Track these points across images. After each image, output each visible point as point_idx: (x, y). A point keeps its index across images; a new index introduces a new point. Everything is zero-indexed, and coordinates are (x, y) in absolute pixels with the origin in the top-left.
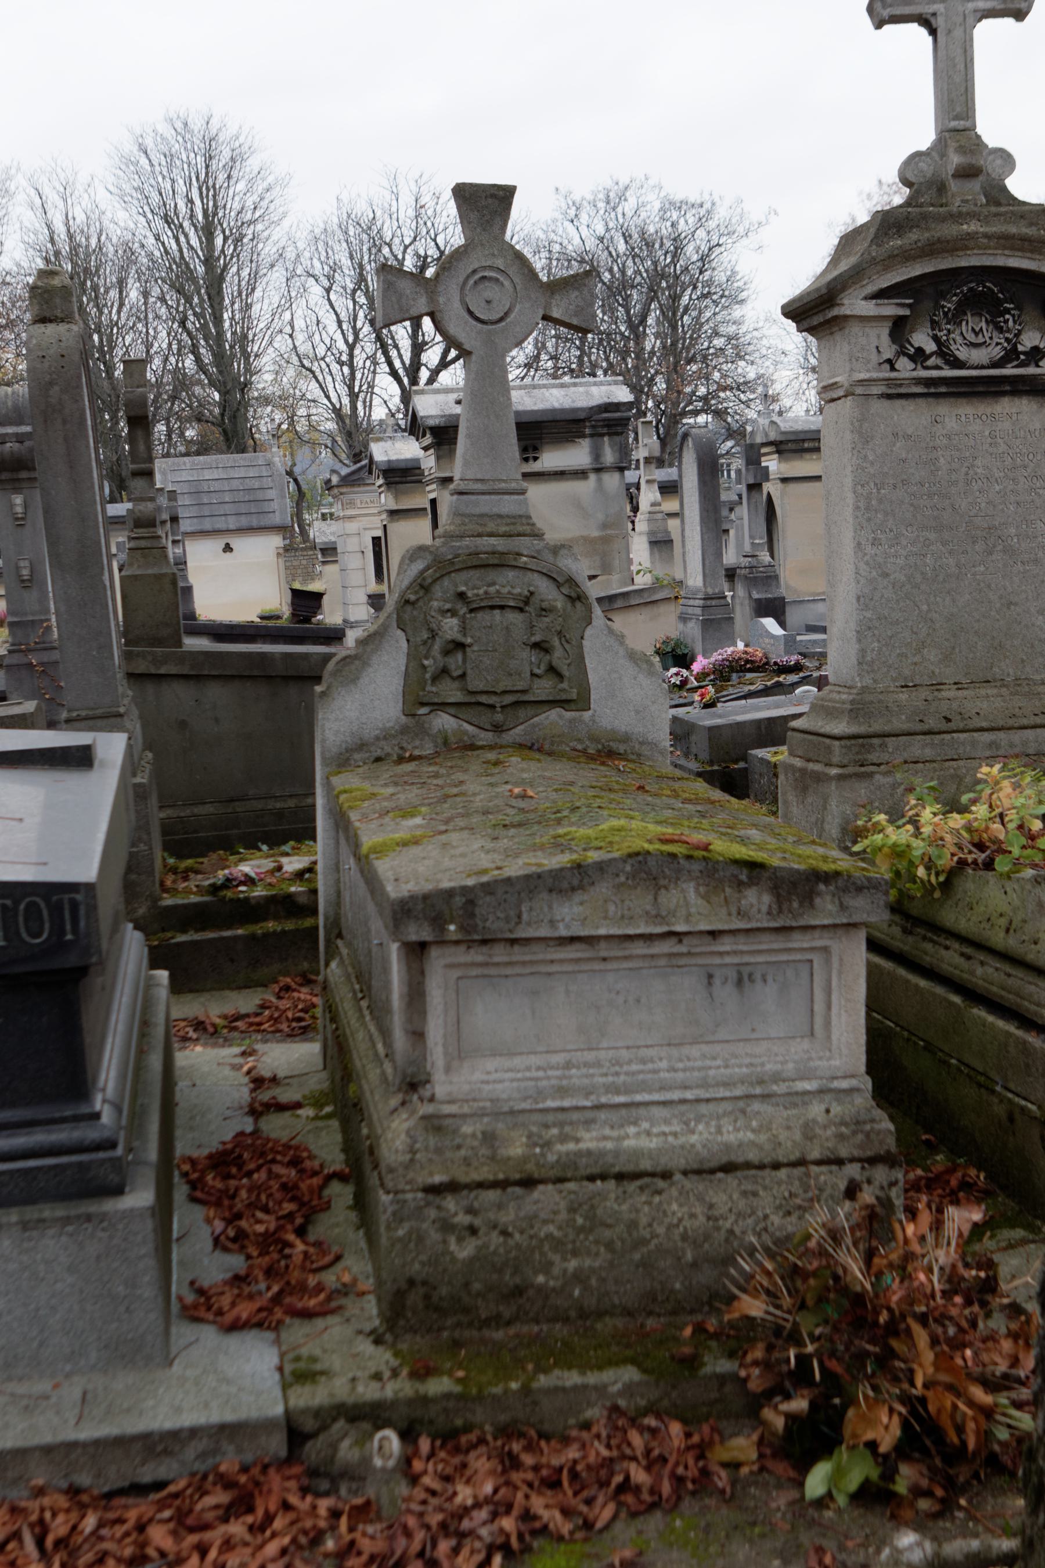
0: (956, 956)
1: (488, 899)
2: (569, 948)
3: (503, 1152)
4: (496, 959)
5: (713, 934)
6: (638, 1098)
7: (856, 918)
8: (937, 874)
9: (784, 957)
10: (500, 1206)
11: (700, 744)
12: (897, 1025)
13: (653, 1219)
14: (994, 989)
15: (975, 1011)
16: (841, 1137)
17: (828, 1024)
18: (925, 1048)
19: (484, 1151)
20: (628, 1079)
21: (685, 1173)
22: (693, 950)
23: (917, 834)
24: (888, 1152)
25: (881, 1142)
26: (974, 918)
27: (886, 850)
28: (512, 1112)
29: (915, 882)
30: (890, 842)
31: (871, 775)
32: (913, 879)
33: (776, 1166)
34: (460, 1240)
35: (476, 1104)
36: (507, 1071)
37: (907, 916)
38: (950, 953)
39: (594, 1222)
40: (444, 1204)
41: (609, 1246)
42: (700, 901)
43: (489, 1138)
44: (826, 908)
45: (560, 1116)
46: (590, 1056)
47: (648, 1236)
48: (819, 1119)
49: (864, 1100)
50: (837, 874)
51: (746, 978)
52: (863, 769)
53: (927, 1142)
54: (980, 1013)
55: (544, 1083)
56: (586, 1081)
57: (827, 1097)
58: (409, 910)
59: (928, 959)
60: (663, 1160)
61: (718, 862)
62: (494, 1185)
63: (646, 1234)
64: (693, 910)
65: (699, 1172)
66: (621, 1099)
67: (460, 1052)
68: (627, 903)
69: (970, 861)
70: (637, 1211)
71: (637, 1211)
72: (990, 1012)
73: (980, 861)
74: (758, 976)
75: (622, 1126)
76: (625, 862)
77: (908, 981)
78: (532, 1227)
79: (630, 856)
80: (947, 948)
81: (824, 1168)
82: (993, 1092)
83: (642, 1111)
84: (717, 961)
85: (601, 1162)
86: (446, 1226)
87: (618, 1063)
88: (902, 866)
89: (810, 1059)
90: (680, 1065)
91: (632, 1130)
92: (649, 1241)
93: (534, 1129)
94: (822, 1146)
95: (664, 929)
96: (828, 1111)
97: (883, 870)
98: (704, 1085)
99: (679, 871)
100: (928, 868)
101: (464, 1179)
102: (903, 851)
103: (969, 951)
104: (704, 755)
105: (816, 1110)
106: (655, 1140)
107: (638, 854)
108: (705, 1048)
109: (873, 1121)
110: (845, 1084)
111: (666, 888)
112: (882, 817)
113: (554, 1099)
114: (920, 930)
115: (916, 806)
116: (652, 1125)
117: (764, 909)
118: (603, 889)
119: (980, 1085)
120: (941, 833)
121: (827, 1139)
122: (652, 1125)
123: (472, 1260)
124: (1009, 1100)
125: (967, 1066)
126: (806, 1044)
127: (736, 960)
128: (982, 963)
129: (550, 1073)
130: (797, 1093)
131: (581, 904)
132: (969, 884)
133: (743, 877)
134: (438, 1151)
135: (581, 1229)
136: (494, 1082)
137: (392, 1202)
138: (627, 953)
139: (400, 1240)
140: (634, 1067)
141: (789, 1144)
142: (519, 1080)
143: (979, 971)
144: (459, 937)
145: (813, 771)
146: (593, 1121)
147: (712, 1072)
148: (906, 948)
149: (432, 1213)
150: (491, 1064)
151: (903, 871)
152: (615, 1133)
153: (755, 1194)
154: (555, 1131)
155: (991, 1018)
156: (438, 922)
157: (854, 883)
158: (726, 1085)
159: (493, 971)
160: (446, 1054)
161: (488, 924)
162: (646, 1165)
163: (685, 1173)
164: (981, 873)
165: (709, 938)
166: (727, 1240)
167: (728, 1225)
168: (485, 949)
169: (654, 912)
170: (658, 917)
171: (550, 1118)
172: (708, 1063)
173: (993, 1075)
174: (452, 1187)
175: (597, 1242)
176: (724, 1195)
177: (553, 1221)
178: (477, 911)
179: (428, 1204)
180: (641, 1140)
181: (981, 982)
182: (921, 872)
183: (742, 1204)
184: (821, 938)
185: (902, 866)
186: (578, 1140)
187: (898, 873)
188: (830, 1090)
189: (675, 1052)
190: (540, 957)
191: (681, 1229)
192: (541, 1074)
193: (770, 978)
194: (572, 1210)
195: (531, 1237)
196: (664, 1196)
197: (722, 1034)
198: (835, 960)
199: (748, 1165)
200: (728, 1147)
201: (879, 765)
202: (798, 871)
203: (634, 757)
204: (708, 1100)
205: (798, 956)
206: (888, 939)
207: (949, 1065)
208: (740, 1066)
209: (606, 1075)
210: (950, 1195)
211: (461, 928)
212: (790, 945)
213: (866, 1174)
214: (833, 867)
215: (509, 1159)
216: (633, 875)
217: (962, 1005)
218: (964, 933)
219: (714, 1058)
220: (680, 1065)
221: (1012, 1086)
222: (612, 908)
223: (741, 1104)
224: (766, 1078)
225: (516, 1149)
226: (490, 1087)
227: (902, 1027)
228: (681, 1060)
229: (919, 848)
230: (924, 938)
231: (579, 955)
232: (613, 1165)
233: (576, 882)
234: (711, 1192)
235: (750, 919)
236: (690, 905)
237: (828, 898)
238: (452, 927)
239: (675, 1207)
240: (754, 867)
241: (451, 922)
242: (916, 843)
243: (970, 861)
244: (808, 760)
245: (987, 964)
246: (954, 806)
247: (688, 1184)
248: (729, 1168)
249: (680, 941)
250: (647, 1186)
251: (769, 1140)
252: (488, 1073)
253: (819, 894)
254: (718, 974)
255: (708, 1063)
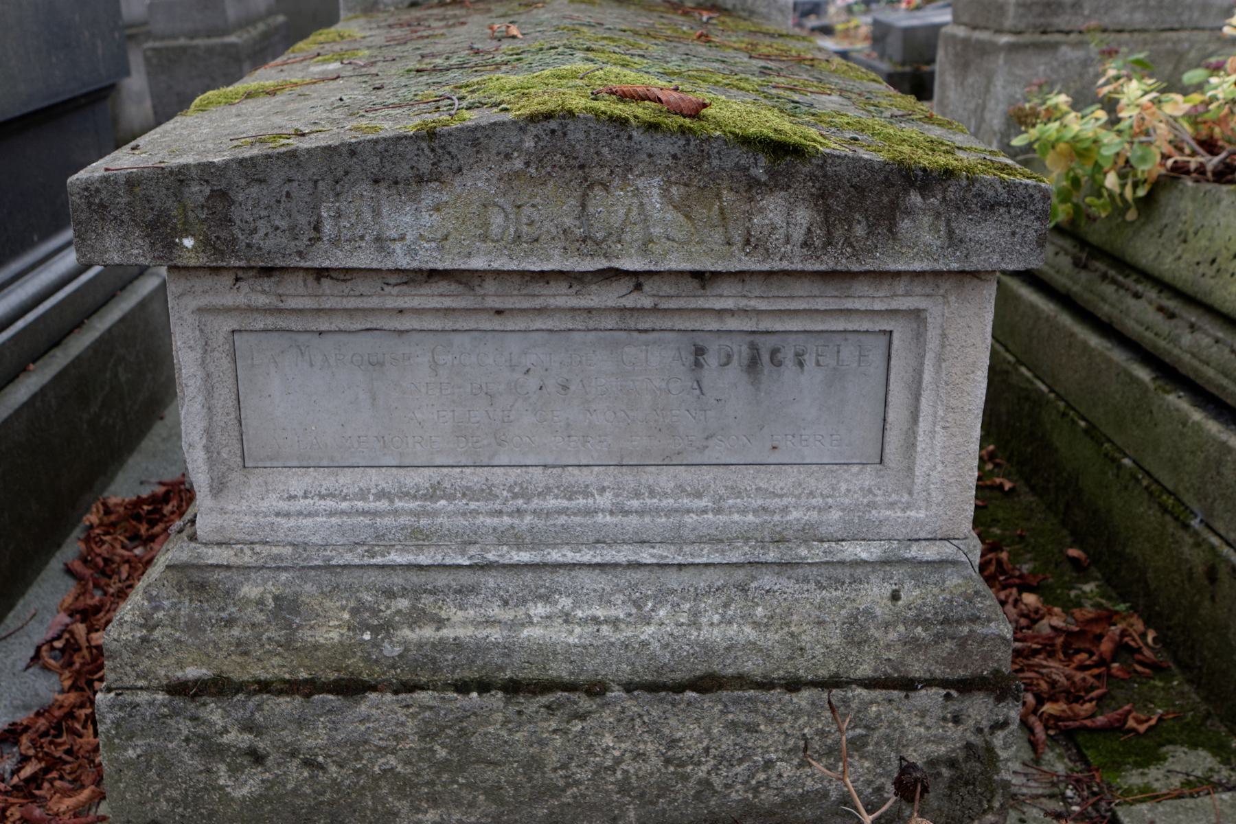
0: (1151, 310)
1: (254, 190)
2: (426, 290)
3: (306, 635)
4: (292, 303)
5: (702, 278)
6: (555, 556)
7: (976, 263)
8: (1135, 186)
9: (839, 325)
10: (301, 723)
11: (894, 45)
12: (1052, 391)
13: (571, 759)
14: (1210, 372)
15: (1171, 398)
16: (913, 644)
17: (910, 446)
18: (1086, 431)
19: (273, 632)
20: (540, 523)
21: (629, 687)
22: (664, 305)
23: (1113, 121)
24: (996, 672)
25: (985, 657)
26: (1186, 256)
27: (1062, 146)
28: (328, 568)
29: (1100, 196)
30: (1069, 135)
31: (1055, 46)
32: (1098, 190)
33: (793, 685)
34: (234, 770)
35: (265, 550)
36: (322, 497)
37: (1082, 243)
38: (1142, 303)
39: (466, 756)
40: (203, 713)
41: (493, 792)
42: (671, 214)
43: (286, 608)
44: (921, 240)
45: (415, 578)
46: (475, 478)
47: (561, 783)
48: (878, 611)
49: (965, 581)
50: (948, 174)
51: (765, 357)
52: (1045, 38)
53: (1074, 561)
54: (1179, 402)
55: (388, 521)
56: (462, 521)
57: (898, 573)
58: (102, 206)
59: (1106, 308)
60: (591, 665)
61: (709, 139)
62: (291, 687)
63: (558, 778)
64: (657, 231)
65: (653, 688)
66: (525, 557)
67: (243, 459)
68: (527, 210)
69: (1193, 166)
70: (542, 743)
71: (542, 743)
72: (1196, 404)
73: (1210, 167)
74: (788, 355)
75: (523, 601)
76: (522, 130)
77: (1072, 335)
78: (358, 757)
79: (533, 118)
80: (1137, 296)
81: (877, 694)
82: (1186, 526)
83: (562, 578)
84: (713, 324)
85: (479, 662)
86: (210, 749)
87: (525, 495)
88: (1083, 172)
89: (872, 505)
90: (635, 503)
91: (539, 610)
92: (564, 790)
93: (367, 597)
94: (877, 657)
95: (601, 264)
96: (895, 596)
97: (1053, 179)
98: (676, 539)
99: (630, 153)
100: (1122, 176)
101: (237, 675)
102: (1087, 149)
103: (1171, 304)
104: (898, 57)
105: (875, 593)
106: (578, 630)
107: (549, 116)
108: (684, 474)
109: (974, 619)
110: (930, 552)
111: (605, 186)
112: (1062, 99)
113: (404, 549)
114: (1101, 266)
115: (1117, 78)
116: (576, 605)
117: (798, 235)
118: (478, 182)
119: (1164, 509)
120: (1150, 122)
121: (888, 647)
122: (576, 605)
123: (255, 801)
124: (1213, 548)
125: (1148, 474)
126: (868, 478)
127: (749, 325)
128: (1192, 327)
129: (399, 504)
130: (842, 563)
131: (437, 209)
132: (1185, 202)
133: (759, 173)
134: (194, 627)
135: (444, 765)
136: (300, 513)
137: (112, 706)
138: (537, 303)
139: (129, 763)
140: (552, 503)
141: (819, 650)
142: (343, 513)
143: (1187, 339)
144: (203, 260)
145: (978, 41)
146: (473, 590)
147: (690, 519)
148: (1076, 288)
149: (185, 727)
150: (297, 483)
151: (1084, 179)
152: (507, 615)
153: (752, 729)
154: (403, 603)
155: (1197, 416)
156: (161, 233)
157: (979, 195)
158: (714, 541)
159: (294, 323)
160: (212, 461)
161: (256, 238)
162: (560, 670)
163: (629, 687)
164: (1209, 186)
165: (695, 283)
166: (698, 796)
167: (702, 772)
168: (267, 283)
169: (579, 232)
170: (586, 242)
171: (398, 580)
172: (686, 502)
173: (1187, 498)
174: (219, 687)
175: (471, 786)
176: (696, 727)
177: (394, 752)
178: (236, 213)
179: (175, 713)
180: (550, 629)
181: (1187, 357)
182: (1111, 181)
183: (727, 742)
184: (907, 294)
185: (1083, 172)
186: (440, 623)
187: (1076, 182)
188: (903, 561)
189: (628, 479)
190: (374, 302)
191: (619, 775)
192: (383, 505)
193: (810, 360)
194: (426, 735)
195: (358, 772)
196: (589, 723)
197: (717, 452)
198: (933, 335)
199: (742, 681)
200: (708, 650)
201: (1068, 33)
202: (868, 164)
203: (745, 14)
204: (680, 566)
205: (866, 325)
206: (1052, 272)
207: (1120, 467)
208: (743, 511)
209: (500, 513)
210: (1097, 665)
211: (205, 244)
212: (849, 304)
213: (953, 707)
214: (942, 160)
215: (316, 647)
216: (538, 158)
217: (1152, 386)
218: (1167, 277)
219: (699, 495)
220: (635, 503)
221: (1219, 526)
222: (497, 220)
223: (740, 575)
224: (789, 534)
225: (330, 633)
226: (292, 522)
227: (1058, 395)
228: (638, 495)
229: (1111, 143)
230: (1104, 277)
231: (448, 302)
232: (501, 668)
233: (425, 167)
234: (673, 722)
235: (768, 254)
236: (650, 221)
237: (926, 220)
238: (188, 242)
239: (608, 740)
240: (780, 150)
241: (186, 233)
242: (1109, 138)
243: (1193, 166)
244: (975, 28)
245: (1200, 328)
246: (1173, 85)
247: (632, 706)
248: (707, 684)
249: (638, 287)
250: (561, 705)
251: (782, 642)
252: (291, 498)
253: (908, 212)
254: (714, 347)
255: (686, 502)
